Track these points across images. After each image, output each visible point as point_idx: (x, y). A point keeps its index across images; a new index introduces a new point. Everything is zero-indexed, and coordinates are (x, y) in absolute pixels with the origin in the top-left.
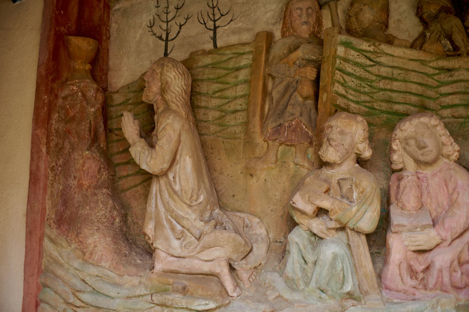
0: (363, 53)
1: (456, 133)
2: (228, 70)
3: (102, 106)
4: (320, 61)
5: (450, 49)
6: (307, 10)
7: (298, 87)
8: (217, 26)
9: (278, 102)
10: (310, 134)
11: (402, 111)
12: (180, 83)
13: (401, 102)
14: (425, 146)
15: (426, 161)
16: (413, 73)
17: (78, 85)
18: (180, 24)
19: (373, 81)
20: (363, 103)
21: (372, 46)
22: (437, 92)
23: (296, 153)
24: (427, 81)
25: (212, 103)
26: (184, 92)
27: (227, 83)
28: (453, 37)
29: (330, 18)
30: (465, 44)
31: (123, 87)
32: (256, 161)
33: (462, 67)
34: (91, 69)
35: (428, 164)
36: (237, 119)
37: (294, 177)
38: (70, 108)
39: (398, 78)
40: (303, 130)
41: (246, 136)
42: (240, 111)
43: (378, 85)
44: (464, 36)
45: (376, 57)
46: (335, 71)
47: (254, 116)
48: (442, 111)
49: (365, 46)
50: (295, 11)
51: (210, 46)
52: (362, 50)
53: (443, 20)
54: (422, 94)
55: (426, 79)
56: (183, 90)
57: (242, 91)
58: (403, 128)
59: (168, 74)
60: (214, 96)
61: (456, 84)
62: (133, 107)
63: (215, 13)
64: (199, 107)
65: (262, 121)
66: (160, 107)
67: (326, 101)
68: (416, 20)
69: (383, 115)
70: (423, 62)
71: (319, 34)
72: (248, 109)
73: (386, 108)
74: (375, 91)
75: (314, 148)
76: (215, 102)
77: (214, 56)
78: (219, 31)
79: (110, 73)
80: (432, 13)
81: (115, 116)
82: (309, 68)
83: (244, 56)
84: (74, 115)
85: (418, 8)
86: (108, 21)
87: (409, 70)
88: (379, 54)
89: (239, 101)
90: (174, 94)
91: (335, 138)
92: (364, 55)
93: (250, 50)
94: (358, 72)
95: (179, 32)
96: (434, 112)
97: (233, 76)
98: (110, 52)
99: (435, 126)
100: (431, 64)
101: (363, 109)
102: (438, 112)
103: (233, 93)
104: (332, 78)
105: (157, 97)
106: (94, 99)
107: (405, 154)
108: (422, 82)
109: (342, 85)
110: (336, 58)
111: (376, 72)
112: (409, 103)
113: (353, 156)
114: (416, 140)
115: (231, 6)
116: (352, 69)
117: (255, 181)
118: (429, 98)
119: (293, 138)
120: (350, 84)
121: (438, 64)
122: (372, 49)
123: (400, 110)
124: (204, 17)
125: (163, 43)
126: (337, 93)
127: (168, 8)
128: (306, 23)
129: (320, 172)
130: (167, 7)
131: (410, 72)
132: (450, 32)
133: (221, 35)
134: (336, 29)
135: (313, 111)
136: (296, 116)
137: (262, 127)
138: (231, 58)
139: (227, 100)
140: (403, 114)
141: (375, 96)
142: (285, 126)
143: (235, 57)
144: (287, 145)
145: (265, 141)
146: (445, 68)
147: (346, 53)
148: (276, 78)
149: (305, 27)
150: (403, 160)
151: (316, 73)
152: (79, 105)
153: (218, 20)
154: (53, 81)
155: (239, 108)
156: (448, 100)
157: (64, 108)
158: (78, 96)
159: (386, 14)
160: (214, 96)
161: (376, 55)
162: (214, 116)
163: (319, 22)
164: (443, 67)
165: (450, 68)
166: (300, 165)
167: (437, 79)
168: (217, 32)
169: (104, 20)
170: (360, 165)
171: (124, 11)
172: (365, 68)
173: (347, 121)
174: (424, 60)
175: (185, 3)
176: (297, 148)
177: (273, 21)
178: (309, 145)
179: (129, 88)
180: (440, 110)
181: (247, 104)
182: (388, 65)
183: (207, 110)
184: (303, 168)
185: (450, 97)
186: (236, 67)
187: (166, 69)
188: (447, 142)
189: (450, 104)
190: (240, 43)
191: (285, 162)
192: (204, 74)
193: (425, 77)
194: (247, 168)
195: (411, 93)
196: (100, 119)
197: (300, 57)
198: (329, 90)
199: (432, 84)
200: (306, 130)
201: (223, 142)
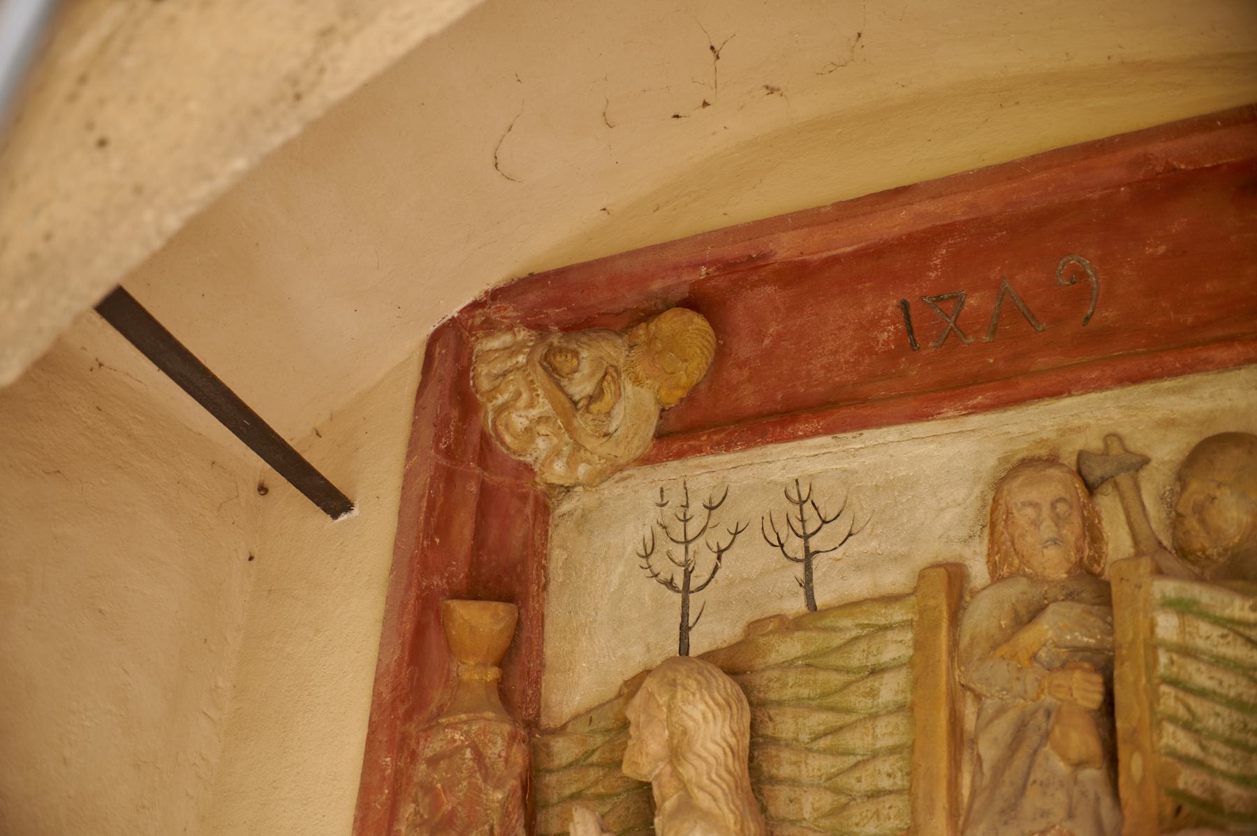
0: (1237, 628)
2: (848, 672)
3: (522, 782)
6: (1053, 506)
7: (1053, 728)
12: (718, 730)
17: (465, 728)
18: (718, 547)
25: (810, 769)
26: (730, 754)
27: (848, 711)
29: (1123, 517)
31: (576, 717)
34: (498, 679)
36: (882, 817)
38: (444, 791)
42: (890, 792)
46: (1159, 685)
47: (931, 811)
50: (1018, 511)
51: (796, 605)
56: (728, 750)
57: (891, 734)
59: (688, 708)
60: (815, 748)
62: (601, 773)
63: (806, 517)
64: (774, 780)
65: (956, 823)
66: (668, 801)
67: (1144, 778)
71: (1095, 566)
72: (911, 787)
76: (817, 766)
77: (808, 634)
78: (816, 561)
79: (548, 679)
81: (555, 799)
83: (890, 635)
84: (454, 808)
86: (543, 544)
89: (885, 765)
90: (704, 764)
92: (1242, 635)
93: (905, 618)
95: (716, 568)
97: (862, 690)
98: (547, 622)
103: (866, 738)
105: (661, 766)
106: (502, 763)
109: (1187, 726)
120: (1211, 722)
125: (678, 598)
126: (1172, 753)
127: (687, 506)
130: (684, 504)
133: (824, 574)
135: (1106, 802)
138: (857, 638)
143: (865, 636)
149: (1052, 552)
151: (1100, 688)
152: (465, 783)
153: (814, 533)
154: (408, 716)
155: (886, 783)
157: (428, 789)
158: (464, 759)
160: (815, 746)
162: (816, 805)
163: (1092, 533)
168: (814, 567)
169: (533, 546)
171: (582, 516)
175: (729, 494)
177: (964, 533)
179: (591, 720)
181: (908, 774)
183: (797, 789)
187: (682, 696)
190: (877, 595)
192: (784, 686)
196: (516, 816)
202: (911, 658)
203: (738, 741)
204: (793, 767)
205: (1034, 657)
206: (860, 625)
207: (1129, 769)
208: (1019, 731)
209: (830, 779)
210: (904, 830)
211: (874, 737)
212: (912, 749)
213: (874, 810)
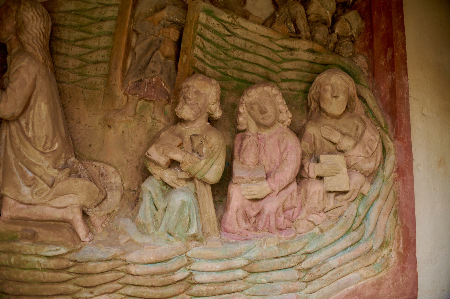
0: (222, 23)
7: (161, 46)
9: (141, 58)
10: (169, 91)
11: (250, 80)
12: (38, 25)
13: (250, 71)
16: (263, 48)
19: (228, 50)
21: (231, 18)
22: (280, 67)
24: (273, 56)
26: (42, 35)
27: (90, 33)
28: (297, 22)
32: (116, 113)
35: (266, 127)
39: (250, 50)
40: (162, 88)
43: (232, 54)
46: (196, 35)
47: (116, 69)
49: (225, 17)
55: (272, 54)
56: (41, 33)
59: (26, 13)
64: (58, 53)
65: (124, 75)
67: (186, 63)
70: (271, 39)
73: (237, 76)
74: (230, 59)
76: (76, 50)
77: (78, 2)
82: (172, 29)
83: (110, 8)
87: (259, 45)
91: (190, 97)
92: (223, 25)
94: (216, 40)
97: (97, 26)
100: (278, 42)
102: (279, 84)
103: (96, 43)
104: (193, 42)
105: (11, 37)
107: (250, 117)
108: (269, 56)
109: (201, 49)
110: (198, 24)
111: (231, 42)
113: (205, 115)
116: (212, 36)
118: (273, 71)
119: (153, 94)
122: (230, 20)
126: (196, 56)
131: (260, 46)
135: (173, 71)
136: (157, 74)
139: (89, 49)
141: (229, 63)
142: (146, 82)
144: (146, 100)
145: (125, 94)
146: (288, 47)
150: (247, 122)
151: (179, 35)
155: (101, 59)
160: (76, 44)
161: (233, 27)
162: (74, 64)
164: (286, 46)
165: (292, 48)
166: (157, 120)
167: (281, 56)
172: (223, 37)
173: (203, 83)
174: (272, 37)
180: (280, 82)
181: (110, 56)
185: (290, 72)
188: (283, 110)
189: (289, 78)
191: (143, 116)
192: (66, 20)
194: (105, 119)
195: (258, 65)
198: (189, 53)
200: (166, 87)
201: (83, 92)
202: (117, 17)
203: (46, 31)
204: (67, 50)
205: (159, 22)
206: (99, 3)
207: (182, 60)
208: (150, 46)
209: (80, 56)
210: (105, 75)
211: (99, 43)
212: (112, 49)
213: (96, 67)
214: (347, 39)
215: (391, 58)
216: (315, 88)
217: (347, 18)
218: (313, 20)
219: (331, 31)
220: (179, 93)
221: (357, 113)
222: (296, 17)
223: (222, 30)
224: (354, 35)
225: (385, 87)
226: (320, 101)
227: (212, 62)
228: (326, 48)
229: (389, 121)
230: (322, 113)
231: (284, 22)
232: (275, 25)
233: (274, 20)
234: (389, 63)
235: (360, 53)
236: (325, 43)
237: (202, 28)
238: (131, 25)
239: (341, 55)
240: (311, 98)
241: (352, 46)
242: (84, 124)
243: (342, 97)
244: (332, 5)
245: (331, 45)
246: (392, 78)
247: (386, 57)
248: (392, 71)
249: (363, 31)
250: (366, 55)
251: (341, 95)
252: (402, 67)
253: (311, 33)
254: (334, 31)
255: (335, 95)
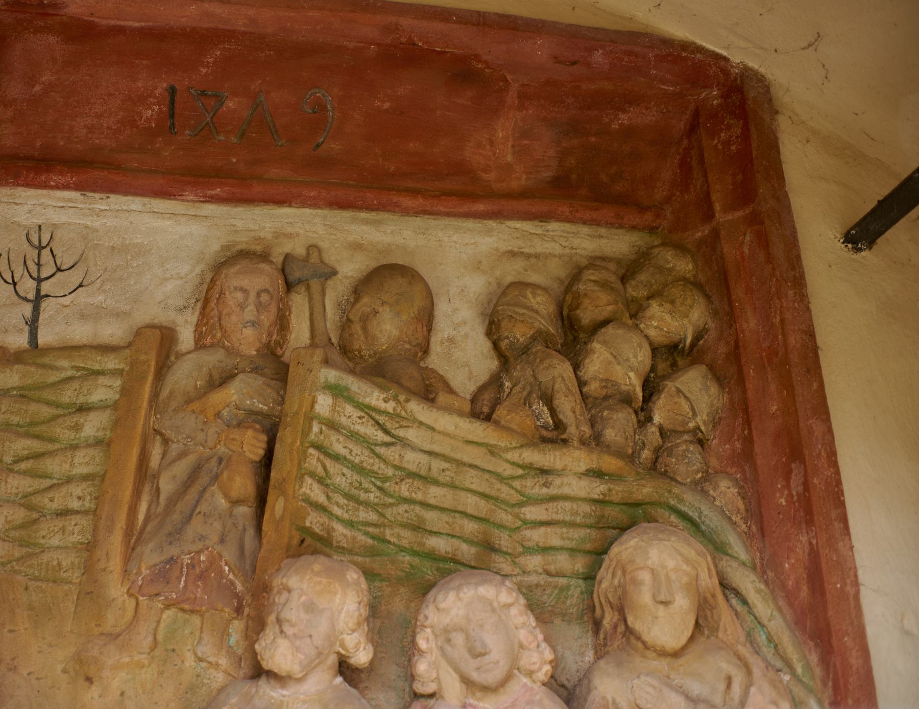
0: (371, 413)
1: (550, 609)
4: (276, 417)
5: (548, 423)
6: (258, 295)
7: (222, 472)
8: (43, 293)
9: (172, 502)
10: (239, 587)
11: (443, 552)
13: (442, 531)
14: (483, 651)
15: (485, 684)
16: (472, 471)
19: (385, 479)
20: (362, 525)
21: (391, 402)
22: (517, 516)
23: (201, 632)
24: (499, 490)
27: (52, 440)
28: (556, 402)
29: (307, 314)
30: (577, 419)
32: (105, 645)
33: (569, 468)
35: (487, 689)
36: (67, 533)
37: (192, 689)
39: (441, 479)
40: (222, 578)
41: (84, 578)
42: (77, 512)
43: (397, 490)
44: (575, 401)
45: (397, 426)
46: (308, 447)
47: (110, 530)
48: (524, 559)
49: (375, 398)
50: (230, 293)
51: (20, 341)
52: (369, 407)
53: (538, 360)
54: (487, 517)
55: (498, 485)
57: (87, 464)
58: (443, 605)
61: (555, 504)
63: (42, 262)
65: (129, 542)
67: (282, 517)
68: (485, 344)
69: (403, 556)
70: (492, 451)
73: (409, 543)
74: (391, 501)
75: (244, 621)
77: (28, 368)
80: (518, 340)
82: (250, 433)
83: (102, 380)
85: (491, 323)
87: (464, 464)
88: (405, 421)
91: (294, 619)
92: (373, 419)
93: (117, 367)
94: (357, 455)
96: (509, 559)
97: (68, 423)
99: (508, 606)
100: (509, 456)
101: (361, 538)
102: (517, 560)
103: (64, 465)
104: (299, 464)
107: (444, 663)
108: (488, 491)
109: (320, 481)
110: (312, 419)
111: (394, 460)
112: (458, 535)
113: (332, 660)
114: (467, 635)
115: (84, 251)
116: (345, 447)
117: (96, 696)
118: (501, 526)
119: (198, 595)
120: (338, 480)
121: (522, 457)
122: (390, 406)
123: (439, 551)
124: (13, 266)
126: (307, 500)
128: (253, 324)
129: (254, 690)
131: (465, 469)
132: (550, 391)
133: (50, 317)
134: (319, 354)
135: (251, 532)
136: (207, 543)
137: (127, 560)
138: (71, 379)
139: (48, 480)
140: (445, 557)
141: (388, 512)
142: (182, 564)
143: (79, 377)
144: (182, 610)
145: (131, 595)
146: (535, 466)
147: (334, 410)
148: (173, 442)
149: (249, 332)
150: (438, 675)
151: (264, 445)
155: (75, 505)
156: (536, 536)
159: (425, 328)
161: (399, 422)
162: (9, 519)
163: (282, 323)
164: (531, 464)
165: (545, 468)
166: (210, 663)
167: (519, 488)
168: (42, 309)
170: (345, 679)
172: (373, 447)
173: (324, 581)
174: (494, 445)
176: (205, 619)
177: (180, 303)
178: (235, 615)
180: (521, 554)
181: (96, 498)
182: (422, 448)
184: (216, 669)
185: (543, 530)
186: (78, 402)
188: (530, 644)
189: (541, 544)
190: (95, 343)
191: (174, 650)
193: (494, 481)
194: (79, 660)
195: (464, 514)
197: (231, 402)
198: (291, 492)
199: (508, 497)
200: (231, 576)
201: (26, 589)
202: (116, 401)
208: (194, 472)
209: (26, 497)
212: (103, 477)
214: (686, 437)
215: (801, 489)
216: (609, 576)
217: (681, 388)
218: (596, 395)
219: (642, 416)
220: (264, 597)
221: (725, 639)
222: (553, 389)
223: (368, 430)
224: (703, 428)
225: (793, 564)
226: (626, 611)
227: (347, 512)
228: (633, 462)
229: (814, 658)
230: (633, 640)
231: (522, 401)
232: (501, 413)
233: (499, 393)
234: (799, 500)
235: (721, 472)
236: (630, 451)
237: (321, 429)
238: (149, 420)
239: (673, 479)
240: (603, 600)
241: (700, 454)
242: (25, 673)
243: (683, 603)
244: (639, 355)
245: (646, 454)
246: (810, 543)
247: (788, 486)
248: (806, 523)
249: (724, 415)
250: (738, 476)
251: (677, 598)
252: (833, 515)
253: (592, 426)
254: (650, 419)
255: (662, 597)
